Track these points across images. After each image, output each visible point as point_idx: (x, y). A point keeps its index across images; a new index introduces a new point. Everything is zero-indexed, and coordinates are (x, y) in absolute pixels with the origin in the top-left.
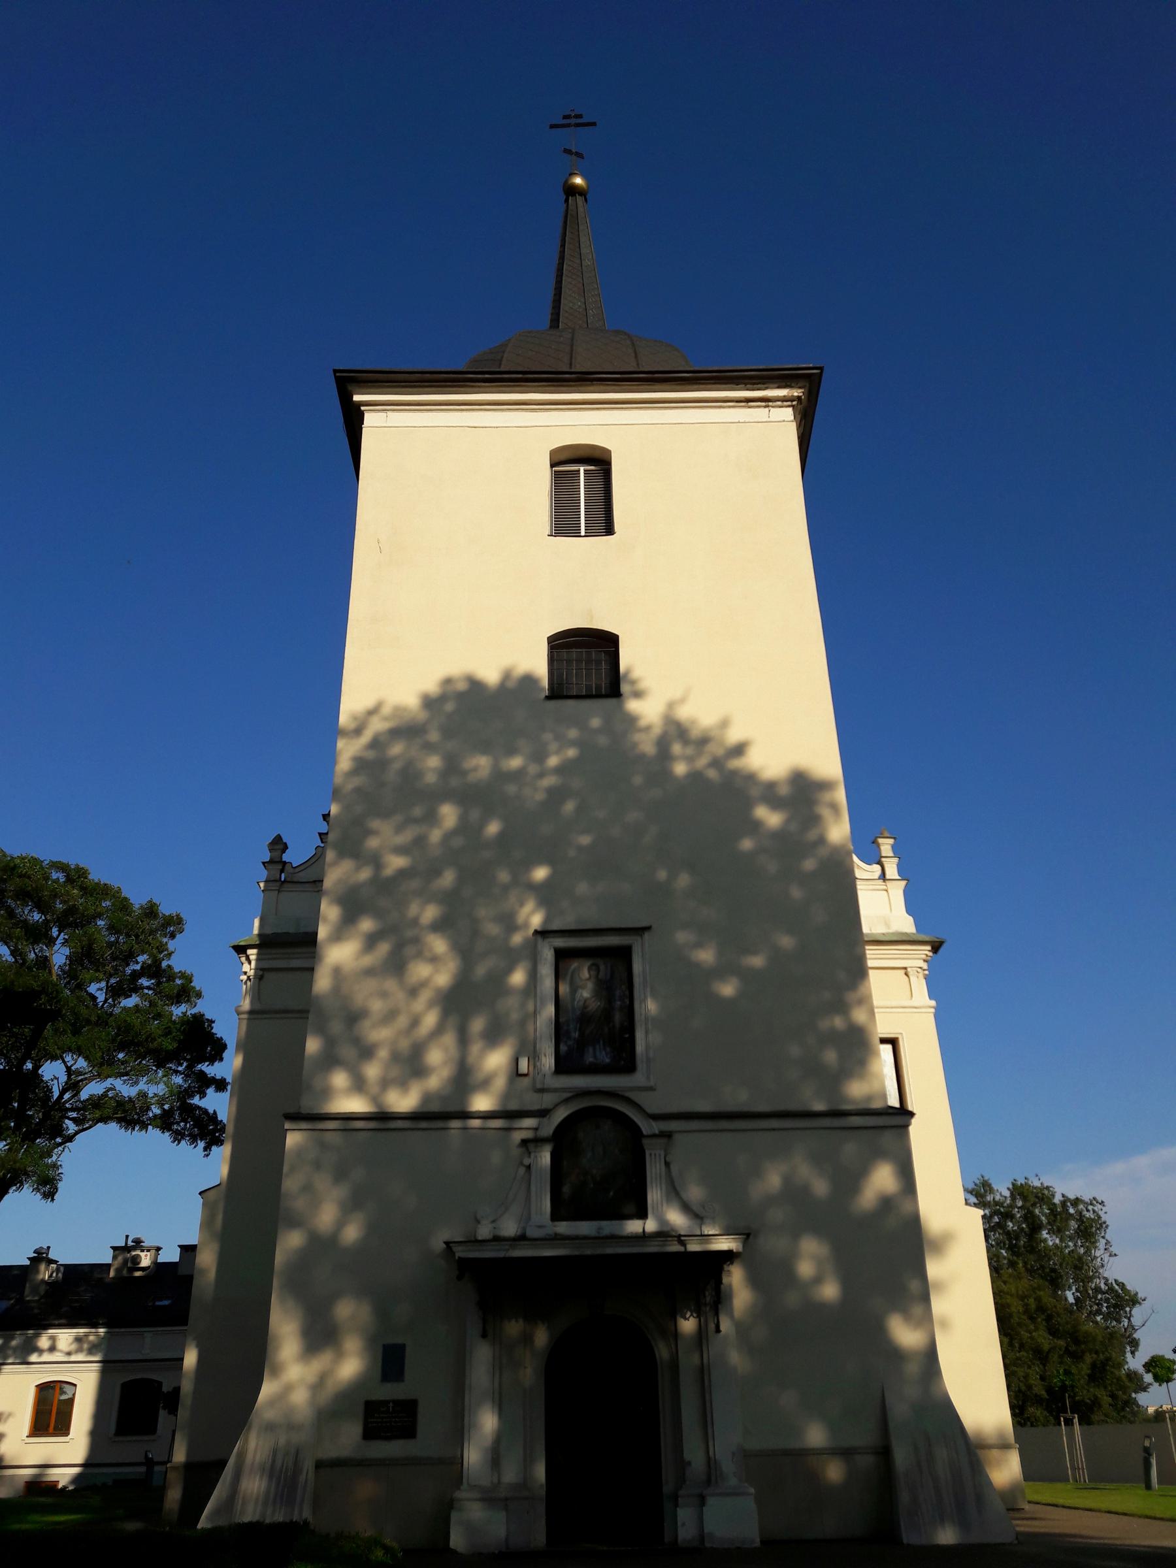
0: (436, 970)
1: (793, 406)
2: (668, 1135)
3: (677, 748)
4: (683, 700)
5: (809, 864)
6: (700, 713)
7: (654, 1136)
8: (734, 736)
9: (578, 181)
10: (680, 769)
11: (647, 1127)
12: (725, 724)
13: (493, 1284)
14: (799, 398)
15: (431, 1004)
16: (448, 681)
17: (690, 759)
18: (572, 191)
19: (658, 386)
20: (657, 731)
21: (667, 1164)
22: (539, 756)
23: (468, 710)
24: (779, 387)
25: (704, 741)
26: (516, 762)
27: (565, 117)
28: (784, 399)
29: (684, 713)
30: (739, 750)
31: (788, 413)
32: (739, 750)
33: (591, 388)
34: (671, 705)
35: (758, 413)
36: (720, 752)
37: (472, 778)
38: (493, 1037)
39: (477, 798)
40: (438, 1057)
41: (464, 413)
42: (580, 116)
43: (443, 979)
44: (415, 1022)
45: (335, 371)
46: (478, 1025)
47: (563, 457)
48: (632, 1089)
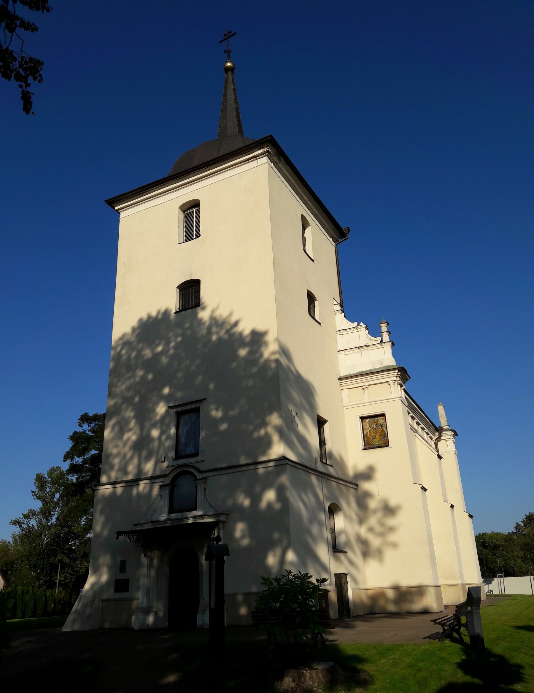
0: (132, 436)
1: (267, 155)
2: (205, 478)
3: (214, 329)
4: (217, 308)
5: (255, 370)
6: (222, 313)
7: (201, 479)
8: (233, 319)
9: (229, 64)
10: (214, 338)
11: (199, 476)
12: (231, 314)
13: (150, 538)
14: (268, 151)
15: (130, 448)
16: (141, 320)
17: (218, 333)
18: (227, 69)
19: (214, 166)
20: (207, 324)
21: (205, 489)
22: (168, 343)
23: (151, 329)
24: (259, 150)
25: (224, 323)
26: (160, 349)
27: (225, 35)
28: (262, 154)
29: (217, 314)
30: (236, 324)
31: (265, 159)
32: (236, 324)
33: (190, 176)
34: (213, 311)
35: (254, 163)
36: (228, 327)
37: (146, 357)
38: (148, 458)
39: (150, 365)
40: (132, 468)
41: (233, 170)
42: (230, 32)
43: (134, 438)
44: (125, 455)
45: (105, 201)
46: (144, 453)
47: (187, 207)
48: (197, 462)
